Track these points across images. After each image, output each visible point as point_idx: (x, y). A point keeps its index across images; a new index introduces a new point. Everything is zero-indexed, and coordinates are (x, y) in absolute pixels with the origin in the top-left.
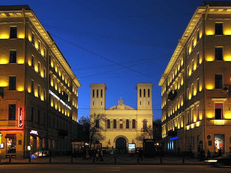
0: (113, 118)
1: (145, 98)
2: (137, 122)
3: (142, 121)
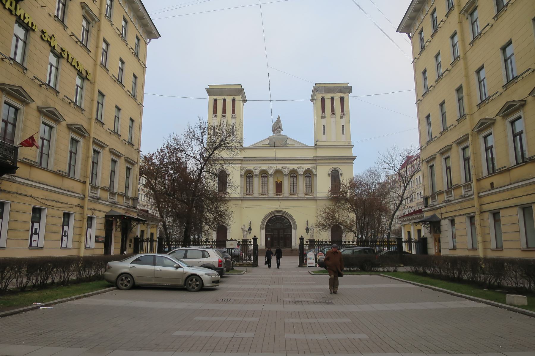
0: (260, 167)
1: (333, 119)
2: (316, 175)
3: (329, 174)
